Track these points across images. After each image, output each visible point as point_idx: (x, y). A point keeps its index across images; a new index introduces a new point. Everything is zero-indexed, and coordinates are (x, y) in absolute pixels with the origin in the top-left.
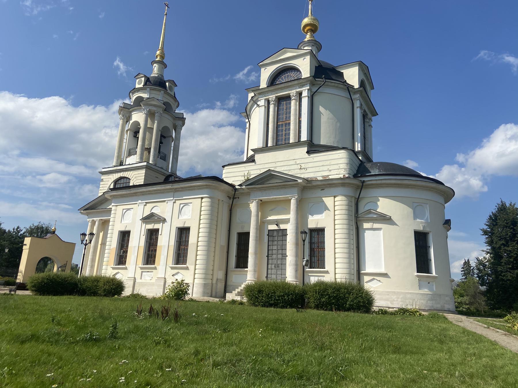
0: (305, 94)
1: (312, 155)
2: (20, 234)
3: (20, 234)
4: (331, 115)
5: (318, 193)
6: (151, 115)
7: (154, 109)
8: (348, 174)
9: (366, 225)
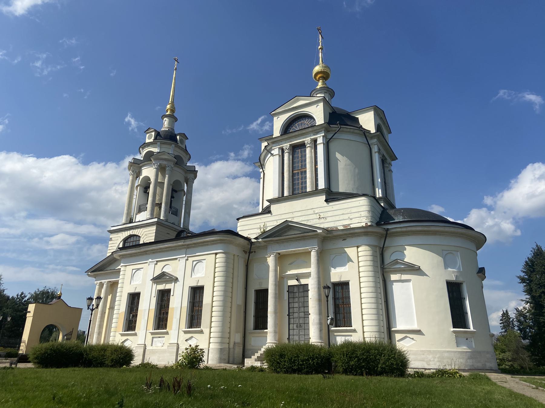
0: (320, 140)
1: (331, 204)
2: (24, 300)
3: (24, 300)
4: (349, 162)
5: (340, 243)
6: (161, 169)
7: (164, 163)
8: (371, 222)
9: (393, 277)
